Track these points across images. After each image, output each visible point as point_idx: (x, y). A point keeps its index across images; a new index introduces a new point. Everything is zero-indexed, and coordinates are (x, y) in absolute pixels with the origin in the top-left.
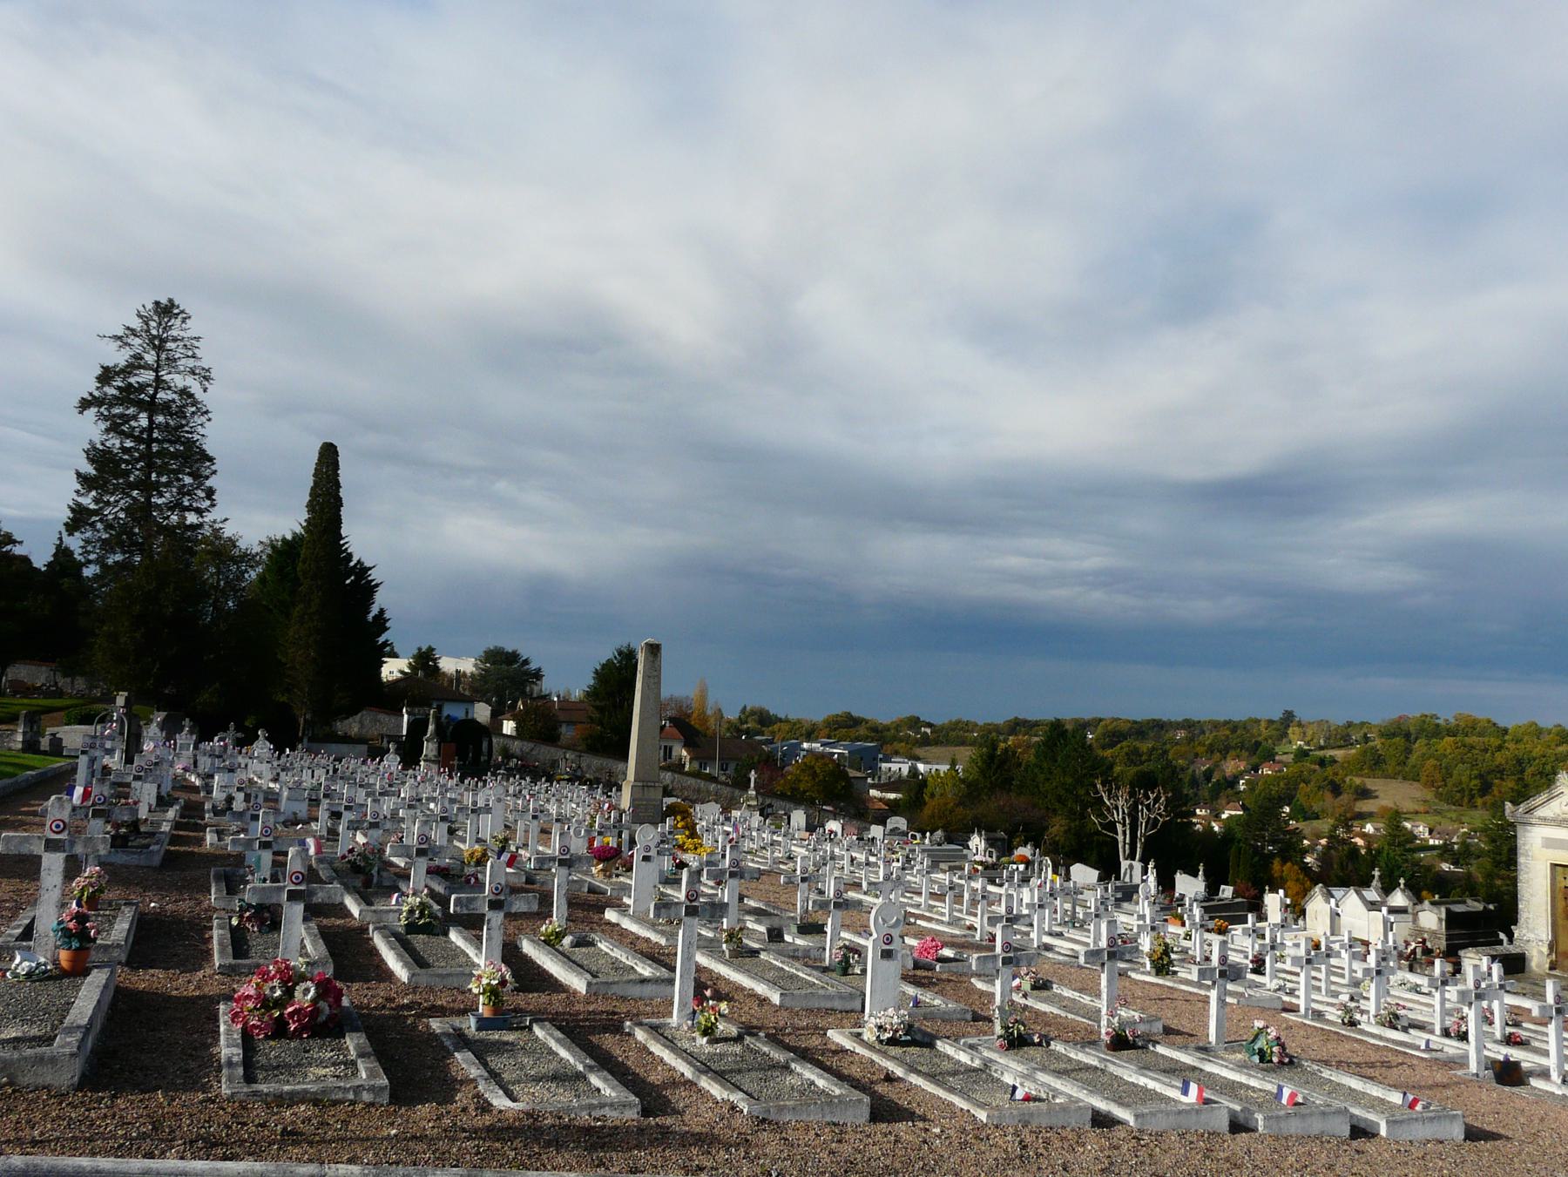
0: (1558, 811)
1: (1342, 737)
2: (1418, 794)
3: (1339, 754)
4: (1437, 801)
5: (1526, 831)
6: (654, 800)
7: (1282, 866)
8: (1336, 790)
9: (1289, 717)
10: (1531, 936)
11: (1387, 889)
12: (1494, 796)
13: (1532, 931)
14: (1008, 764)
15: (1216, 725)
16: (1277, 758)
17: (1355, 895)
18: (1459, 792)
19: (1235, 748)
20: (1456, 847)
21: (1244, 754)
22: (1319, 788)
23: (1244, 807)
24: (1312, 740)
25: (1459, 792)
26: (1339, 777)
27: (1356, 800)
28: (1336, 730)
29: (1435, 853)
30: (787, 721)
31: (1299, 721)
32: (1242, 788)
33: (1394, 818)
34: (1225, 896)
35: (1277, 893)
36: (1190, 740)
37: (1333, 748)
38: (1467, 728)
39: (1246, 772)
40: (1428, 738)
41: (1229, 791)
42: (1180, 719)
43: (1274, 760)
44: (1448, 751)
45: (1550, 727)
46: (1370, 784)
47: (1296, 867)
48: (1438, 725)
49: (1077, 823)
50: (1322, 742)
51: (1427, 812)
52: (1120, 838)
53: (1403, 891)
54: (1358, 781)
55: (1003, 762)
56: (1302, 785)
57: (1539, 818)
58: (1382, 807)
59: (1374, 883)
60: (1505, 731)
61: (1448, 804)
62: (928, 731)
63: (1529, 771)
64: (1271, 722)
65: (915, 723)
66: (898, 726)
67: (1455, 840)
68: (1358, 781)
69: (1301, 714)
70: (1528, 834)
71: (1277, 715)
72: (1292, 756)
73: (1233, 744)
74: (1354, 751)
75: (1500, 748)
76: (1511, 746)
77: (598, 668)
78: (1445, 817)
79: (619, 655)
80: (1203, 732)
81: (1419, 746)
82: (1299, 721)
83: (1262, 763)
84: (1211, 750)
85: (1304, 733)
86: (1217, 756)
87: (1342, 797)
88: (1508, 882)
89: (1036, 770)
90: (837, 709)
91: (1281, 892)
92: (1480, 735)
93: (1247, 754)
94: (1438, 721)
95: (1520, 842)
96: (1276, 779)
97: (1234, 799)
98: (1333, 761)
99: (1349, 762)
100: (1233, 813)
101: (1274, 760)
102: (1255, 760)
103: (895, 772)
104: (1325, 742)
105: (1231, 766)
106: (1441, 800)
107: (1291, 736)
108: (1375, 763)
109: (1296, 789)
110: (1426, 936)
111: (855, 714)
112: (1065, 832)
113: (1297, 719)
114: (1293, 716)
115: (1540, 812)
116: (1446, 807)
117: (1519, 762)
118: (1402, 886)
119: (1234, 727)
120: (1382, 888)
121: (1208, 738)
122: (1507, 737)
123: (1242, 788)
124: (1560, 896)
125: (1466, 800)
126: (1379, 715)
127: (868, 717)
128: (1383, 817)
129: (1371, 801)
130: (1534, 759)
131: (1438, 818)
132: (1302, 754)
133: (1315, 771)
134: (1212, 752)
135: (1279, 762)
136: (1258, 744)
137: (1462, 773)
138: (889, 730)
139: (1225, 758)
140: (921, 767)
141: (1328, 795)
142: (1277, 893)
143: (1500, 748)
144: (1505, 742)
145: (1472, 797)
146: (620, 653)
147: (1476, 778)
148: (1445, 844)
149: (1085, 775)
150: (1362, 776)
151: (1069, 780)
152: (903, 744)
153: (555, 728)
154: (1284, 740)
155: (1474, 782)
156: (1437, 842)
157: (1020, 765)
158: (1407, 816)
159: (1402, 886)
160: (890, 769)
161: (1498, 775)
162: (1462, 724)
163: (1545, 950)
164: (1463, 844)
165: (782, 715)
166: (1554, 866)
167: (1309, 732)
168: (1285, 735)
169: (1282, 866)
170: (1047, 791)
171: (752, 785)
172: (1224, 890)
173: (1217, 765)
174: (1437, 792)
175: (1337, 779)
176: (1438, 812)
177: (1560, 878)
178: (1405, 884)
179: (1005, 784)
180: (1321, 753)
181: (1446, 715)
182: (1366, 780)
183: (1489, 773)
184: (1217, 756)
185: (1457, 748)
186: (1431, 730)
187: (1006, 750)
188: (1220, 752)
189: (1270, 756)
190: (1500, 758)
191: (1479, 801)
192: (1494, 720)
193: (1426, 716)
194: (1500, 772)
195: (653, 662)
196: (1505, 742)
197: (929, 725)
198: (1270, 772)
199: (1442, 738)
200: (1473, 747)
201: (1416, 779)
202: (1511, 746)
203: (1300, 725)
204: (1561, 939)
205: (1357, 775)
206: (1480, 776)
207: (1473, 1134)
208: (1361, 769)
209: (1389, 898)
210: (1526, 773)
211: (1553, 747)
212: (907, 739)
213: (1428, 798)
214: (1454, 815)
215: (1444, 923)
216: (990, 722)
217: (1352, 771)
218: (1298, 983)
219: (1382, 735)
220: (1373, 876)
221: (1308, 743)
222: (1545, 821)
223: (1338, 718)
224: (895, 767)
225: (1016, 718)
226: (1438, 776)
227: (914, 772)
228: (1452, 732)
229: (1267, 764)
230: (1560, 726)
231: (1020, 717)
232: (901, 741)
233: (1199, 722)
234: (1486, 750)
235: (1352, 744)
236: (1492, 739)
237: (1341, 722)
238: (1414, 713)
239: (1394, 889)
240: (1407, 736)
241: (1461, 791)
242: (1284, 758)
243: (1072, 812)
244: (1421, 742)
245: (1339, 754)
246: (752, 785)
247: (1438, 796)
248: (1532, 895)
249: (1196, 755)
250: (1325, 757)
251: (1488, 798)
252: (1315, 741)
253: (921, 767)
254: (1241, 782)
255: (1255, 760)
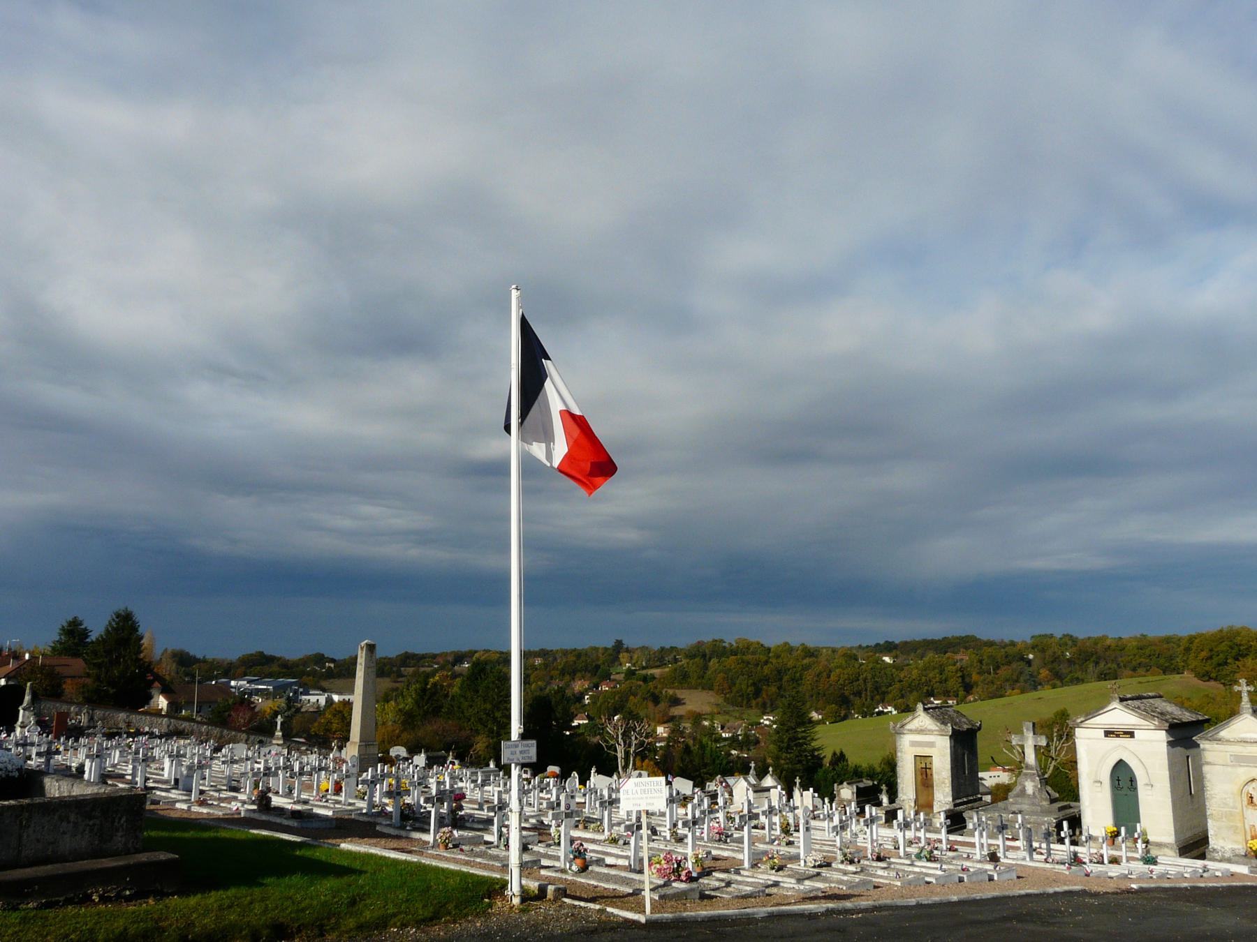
0: (917, 725)
1: (661, 657)
2: (712, 700)
3: (656, 672)
4: (725, 704)
5: (901, 737)
6: (373, 754)
7: (642, 763)
8: (656, 699)
9: (619, 644)
10: (905, 797)
11: (761, 775)
12: (763, 698)
13: (905, 794)
14: (438, 695)
15: (565, 653)
16: (612, 677)
17: (743, 781)
18: (740, 696)
19: (580, 671)
20: (740, 738)
21: (588, 675)
22: (644, 699)
23: (588, 717)
24: (637, 662)
25: (740, 696)
26: (658, 690)
27: (670, 706)
28: (654, 653)
29: (726, 743)
30: (204, 661)
31: (627, 648)
32: (587, 702)
33: (697, 718)
34: (710, 789)
35: (809, 790)
36: (546, 665)
37: (652, 668)
38: (743, 650)
39: (590, 689)
40: (719, 657)
41: (578, 705)
42: (537, 649)
43: (610, 679)
44: (733, 667)
45: (798, 646)
46: (681, 694)
47: (652, 763)
48: (725, 647)
49: (495, 740)
50: (644, 664)
51: (719, 713)
52: (619, 755)
53: (772, 776)
54: (671, 692)
55: (434, 694)
56: (632, 697)
57: (908, 730)
58: (689, 711)
59: (752, 771)
60: (769, 649)
61: (733, 706)
62: (332, 665)
63: (786, 678)
64: (606, 649)
65: (320, 659)
66: (305, 661)
67: (739, 733)
68: (671, 692)
69: (629, 642)
70: (902, 740)
71: (610, 644)
72: (623, 675)
73: (579, 668)
74: (667, 670)
75: (766, 663)
76: (774, 661)
77: (65, 624)
78: (731, 716)
79: (117, 618)
80: (555, 659)
81: (713, 663)
82: (627, 648)
83: (601, 681)
84: (563, 673)
85: (631, 657)
86: (567, 677)
87: (660, 705)
88: (788, 761)
89: (462, 700)
90: (251, 648)
91: (811, 789)
92: (753, 653)
93: (589, 675)
94: (724, 644)
95: (898, 744)
96: (613, 694)
97: (581, 710)
98: (653, 678)
99: (664, 678)
100: (581, 722)
101: (610, 679)
102: (595, 680)
103: (314, 703)
104: (646, 663)
105: (578, 686)
106: (728, 703)
107: (622, 660)
108: (682, 678)
109: (627, 701)
110: (845, 803)
111: (268, 652)
112: (487, 747)
113: (625, 646)
114: (623, 644)
115: (908, 727)
116: (731, 709)
117: (779, 672)
118: (771, 773)
119: (579, 654)
120: (756, 775)
121: (561, 662)
122: (771, 655)
123: (587, 702)
124: (919, 773)
125: (745, 702)
126: (684, 642)
127: (278, 655)
128: (689, 719)
129: (680, 707)
130: (789, 670)
131: (727, 717)
132: (630, 673)
133: (640, 686)
134: (564, 675)
135: (614, 680)
136: (598, 667)
137: (743, 684)
138: (298, 666)
139: (574, 679)
140: (336, 698)
141: (651, 705)
142: (809, 790)
143: (766, 663)
144: (769, 658)
145: (749, 700)
146: (118, 616)
147: (751, 685)
148: (733, 736)
149: (501, 702)
150: (673, 688)
151: (488, 706)
152: (311, 678)
153: (59, 685)
154: (616, 664)
155: (750, 689)
156: (727, 735)
157: (446, 696)
158: (706, 716)
159: (771, 773)
160: (309, 700)
161: (766, 683)
162: (741, 646)
163: (913, 804)
164: (746, 736)
165: (199, 656)
166: (916, 756)
167: (635, 657)
168: (617, 658)
169: (642, 763)
170: (470, 716)
171: (279, 727)
172: (709, 786)
173: (568, 685)
174: (725, 698)
175: (656, 691)
176: (727, 713)
177: (918, 763)
178: (773, 771)
179: (436, 711)
180: (644, 672)
181: (730, 639)
182: (677, 691)
183: (760, 681)
184: (567, 677)
185: (738, 664)
186: (718, 650)
187: (435, 684)
188: (570, 674)
189: (606, 677)
190: (766, 670)
191: (754, 703)
192: (762, 642)
193: (716, 641)
194: (767, 680)
195: (371, 657)
196: (769, 658)
197: (333, 661)
198: (607, 689)
199: (728, 657)
200: (748, 663)
201: (711, 688)
202: (774, 661)
203: (628, 650)
204: (919, 797)
205: (671, 688)
206: (754, 684)
207: (1018, 877)
208: (673, 683)
209: (763, 781)
210: (783, 681)
211: (800, 660)
212: (314, 673)
213: (720, 702)
214: (737, 715)
215: (855, 795)
216: (384, 656)
217: (666, 685)
218: (799, 838)
219: (687, 656)
220: (751, 767)
221: (634, 665)
222: (911, 731)
223: (656, 643)
224: (313, 699)
225: (406, 653)
226: (726, 686)
227: (330, 701)
228: (734, 652)
229: (605, 682)
230: (804, 644)
231: (409, 651)
232: (309, 675)
233: (552, 651)
234: (757, 665)
235: (665, 664)
236: (761, 656)
237: (656, 647)
238: (707, 638)
239: (766, 775)
240: (704, 656)
241: (742, 696)
242: (617, 677)
243: (491, 731)
244: (714, 661)
245: (656, 672)
246: (279, 727)
247: (726, 700)
248: (905, 774)
249: (552, 678)
250: (647, 675)
251: (760, 700)
252: (639, 663)
253: (336, 698)
254: (586, 697)
255: (595, 680)
